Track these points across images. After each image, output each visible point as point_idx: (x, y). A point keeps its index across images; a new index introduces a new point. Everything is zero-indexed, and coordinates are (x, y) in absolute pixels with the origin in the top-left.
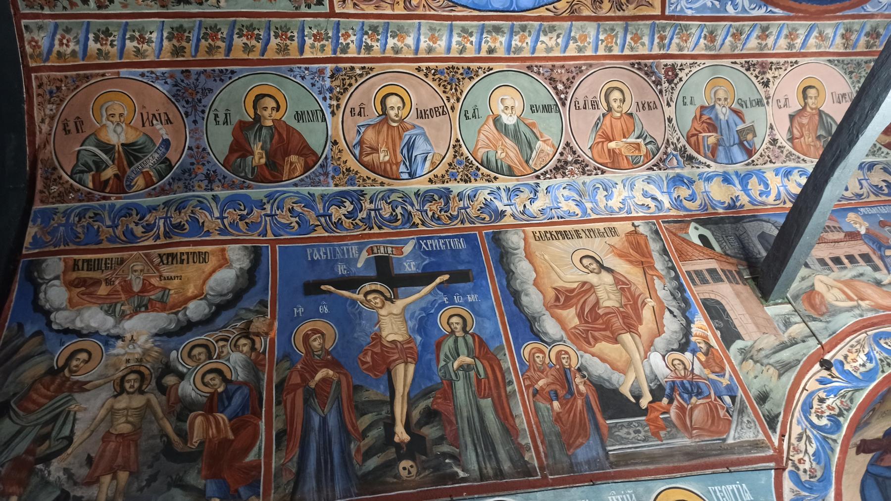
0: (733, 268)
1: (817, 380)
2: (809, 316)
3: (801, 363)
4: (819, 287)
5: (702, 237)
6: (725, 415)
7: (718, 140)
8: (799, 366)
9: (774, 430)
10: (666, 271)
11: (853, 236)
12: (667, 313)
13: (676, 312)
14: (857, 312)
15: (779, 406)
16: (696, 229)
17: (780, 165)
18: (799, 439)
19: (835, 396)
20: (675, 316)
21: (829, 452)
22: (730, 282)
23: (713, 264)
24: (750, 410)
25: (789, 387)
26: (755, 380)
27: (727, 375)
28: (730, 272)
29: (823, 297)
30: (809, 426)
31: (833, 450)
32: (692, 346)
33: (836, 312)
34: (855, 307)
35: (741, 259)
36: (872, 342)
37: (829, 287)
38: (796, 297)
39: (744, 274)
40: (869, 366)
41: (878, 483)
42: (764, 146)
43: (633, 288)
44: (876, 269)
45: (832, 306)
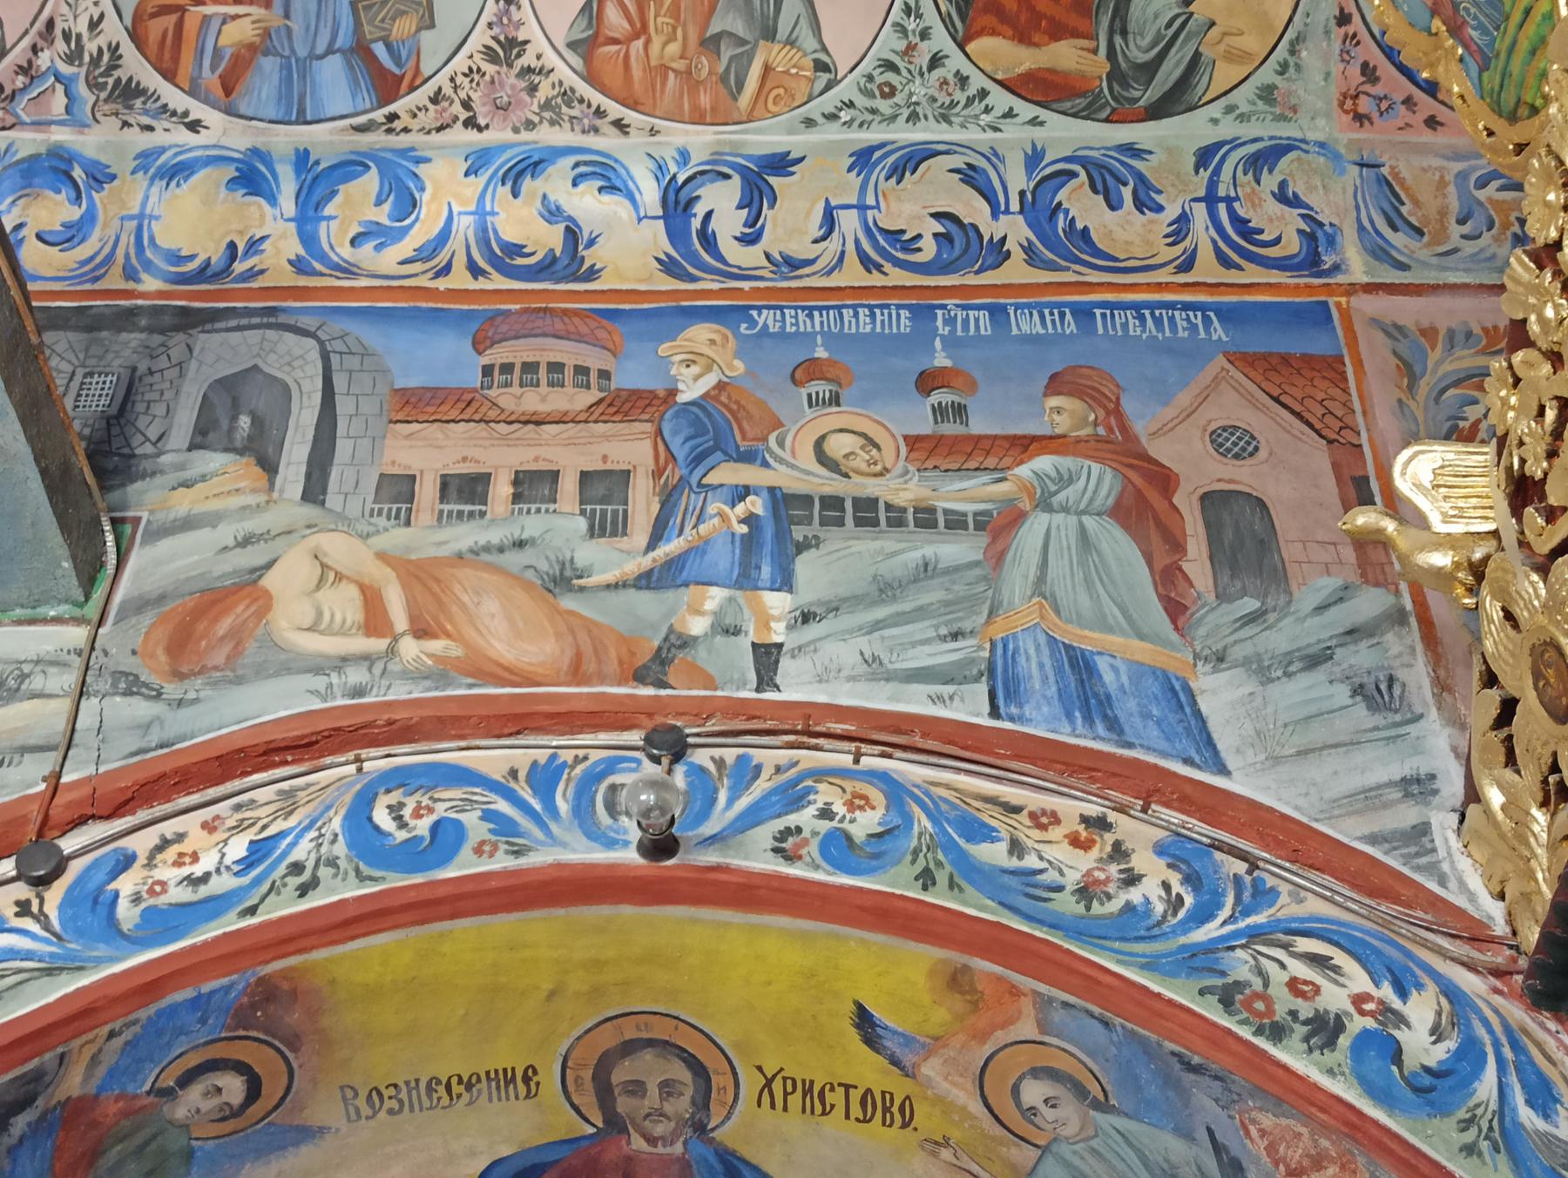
7: (267, 34)
17: (508, 136)
34: (367, 659)
42: (460, 63)
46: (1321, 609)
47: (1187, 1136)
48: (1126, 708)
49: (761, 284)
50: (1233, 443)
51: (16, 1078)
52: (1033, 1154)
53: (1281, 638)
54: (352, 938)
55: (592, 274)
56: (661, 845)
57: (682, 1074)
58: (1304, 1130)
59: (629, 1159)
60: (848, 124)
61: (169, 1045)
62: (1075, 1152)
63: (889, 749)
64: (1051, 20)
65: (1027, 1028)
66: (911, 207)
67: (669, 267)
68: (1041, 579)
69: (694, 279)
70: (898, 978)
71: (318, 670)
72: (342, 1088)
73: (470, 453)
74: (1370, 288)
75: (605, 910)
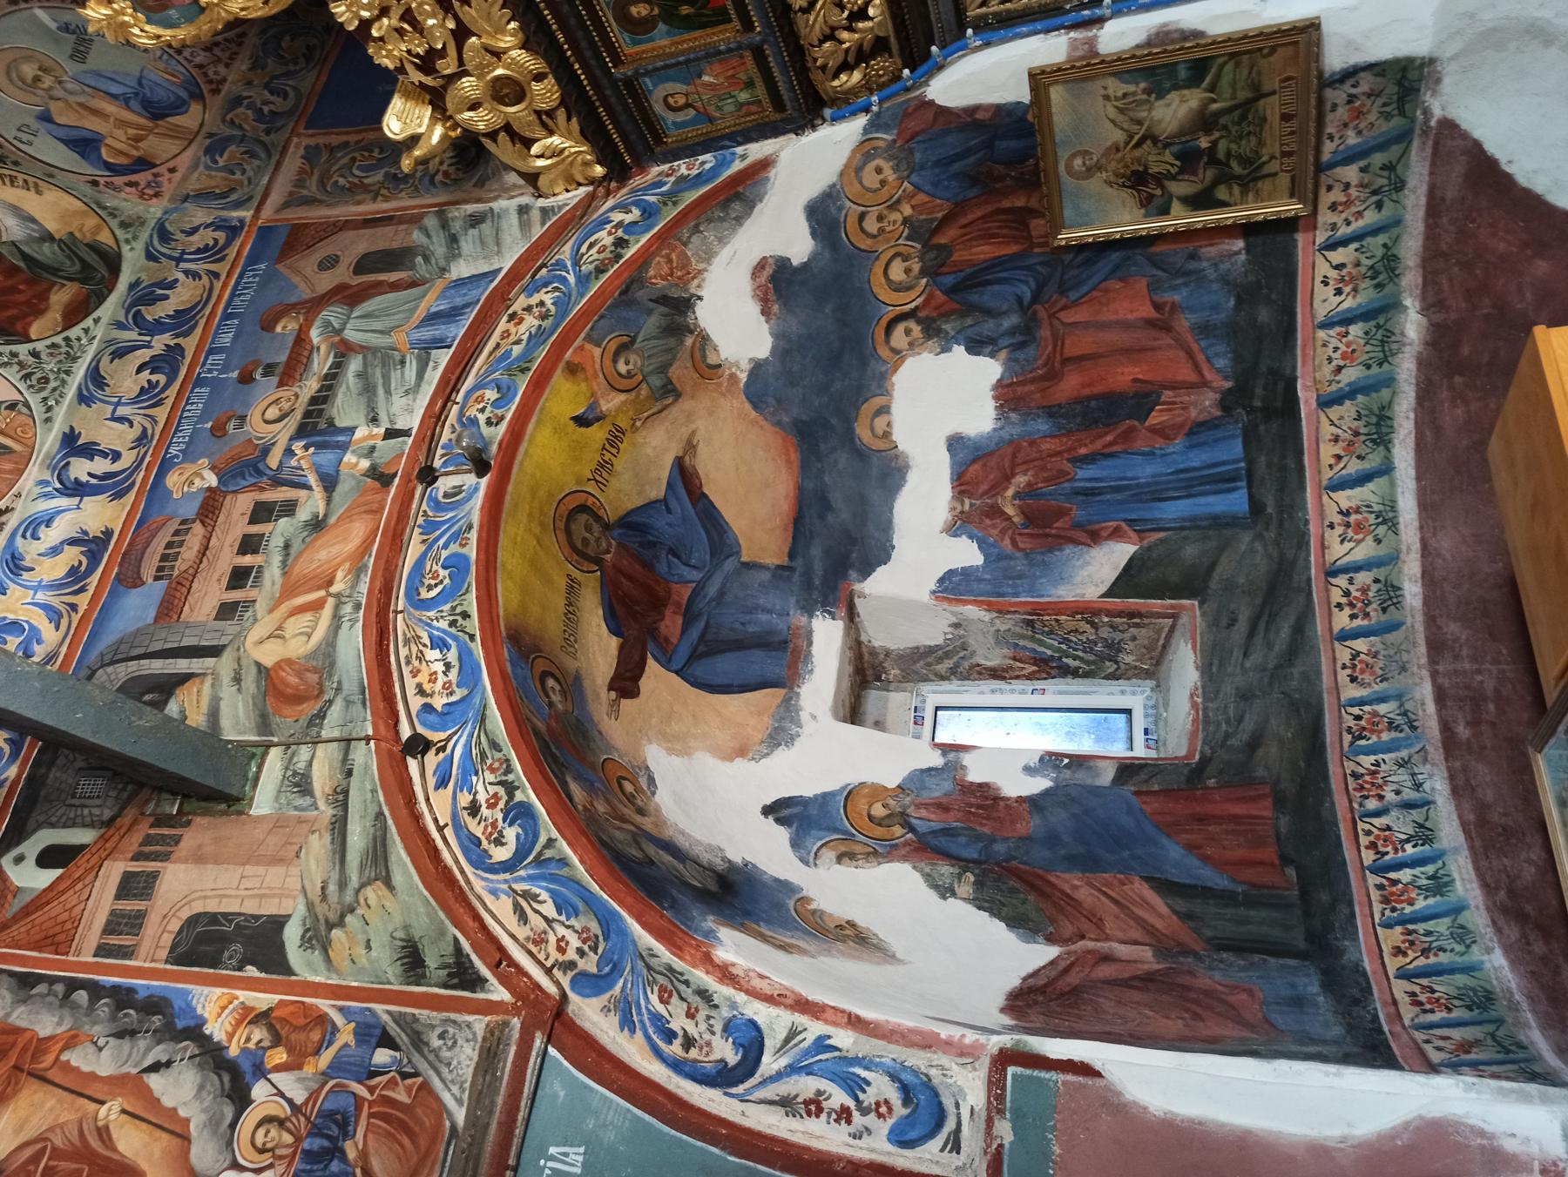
0: (144, 829)
1: (437, 788)
2: (310, 724)
3: (387, 813)
4: (269, 655)
5: (47, 859)
6: (408, 1089)
8: (390, 822)
9: (477, 982)
10: (66, 1012)
11: (210, 507)
12: (155, 1081)
13: (159, 1053)
14: (347, 609)
15: (442, 932)
16: (19, 859)
18: (523, 918)
19: (477, 774)
20: (168, 1064)
21: (564, 872)
22: (164, 857)
23: (114, 871)
24: (423, 1014)
25: (416, 878)
26: (374, 954)
27: (338, 1019)
28: (148, 840)
29: (289, 662)
30: (507, 876)
31: (563, 862)
32: (246, 1066)
33: (328, 650)
34: (337, 607)
35: (134, 794)
36: (417, 613)
37: (277, 634)
38: (264, 725)
39: (167, 810)
40: (452, 656)
41: (709, 653)
43: (58, 1141)
44: (289, 508)
45: (313, 655)
46: (429, 236)
47: (650, 312)
48: (459, 301)
49: (148, 459)
50: (329, 263)
52: (644, 385)
53: (439, 249)
55: (108, 533)
56: (481, 467)
60: (57, 402)
63: (455, 389)
64: (35, 297)
65: (597, 352)
66: (126, 379)
67: (119, 495)
68: (381, 332)
69: (133, 483)
70: (564, 398)
71: (338, 627)
73: (216, 576)
74: (258, 210)
75: (508, 498)
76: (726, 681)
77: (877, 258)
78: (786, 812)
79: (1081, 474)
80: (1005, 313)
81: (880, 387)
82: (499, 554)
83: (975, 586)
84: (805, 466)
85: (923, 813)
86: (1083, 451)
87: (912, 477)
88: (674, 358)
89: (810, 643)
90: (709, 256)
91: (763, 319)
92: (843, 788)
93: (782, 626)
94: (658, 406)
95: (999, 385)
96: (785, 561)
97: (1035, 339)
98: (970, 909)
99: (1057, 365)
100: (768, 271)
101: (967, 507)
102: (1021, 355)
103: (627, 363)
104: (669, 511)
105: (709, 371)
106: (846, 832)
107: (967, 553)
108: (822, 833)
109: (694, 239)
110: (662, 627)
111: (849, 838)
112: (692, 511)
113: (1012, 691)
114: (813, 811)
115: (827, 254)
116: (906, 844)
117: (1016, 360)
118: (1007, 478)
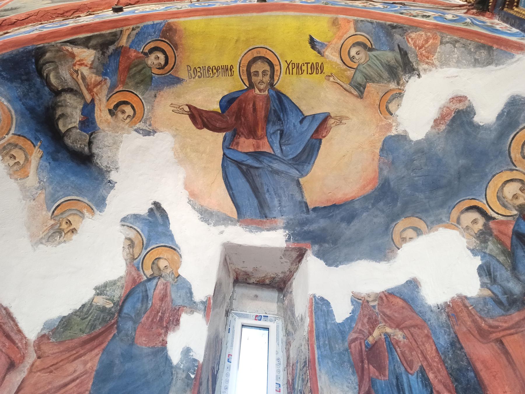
47: (392, 50)
51: (110, 33)
52: (353, 71)
54: (190, 16)
57: (267, 68)
58: (423, 33)
59: (255, 97)
61: (146, 38)
62: (364, 67)
65: (352, 32)
72: (187, 66)
75: (249, 15)
76: (233, 186)
77: (512, 170)
78: (158, 215)
79: (413, 378)
80: (519, 279)
81: (432, 223)
82: (216, 17)
83: (322, 320)
84: (366, 198)
85: (160, 287)
86: (431, 376)
87: (383, 266)
88: (378, 82)
89: (268, 230)
90: (445, 63)
91: (432, 123)
92: (177, 246)
93: (275, 214)
94: (348, 87)
95: (463, 299)
96: (311, 207)
97: (508, 310)
98: (85, 300)
99: (494, 336)
100: (460, 106)
101: (372, 304)
102: (491, 305)
103: (358, 53)
104: (301, 122)
105: (386, 107)
106: (148, 245)
107: (342, 311)
108: (146, 232)
109: (449, 45)
110: (242, 140)
111: (144, 246)
112: (308, 137)
113: (278, 371)
114: (160, 229)
115: (493, 135)
116: (139, 276)
117: (486, 304)
118: (398, 326)
